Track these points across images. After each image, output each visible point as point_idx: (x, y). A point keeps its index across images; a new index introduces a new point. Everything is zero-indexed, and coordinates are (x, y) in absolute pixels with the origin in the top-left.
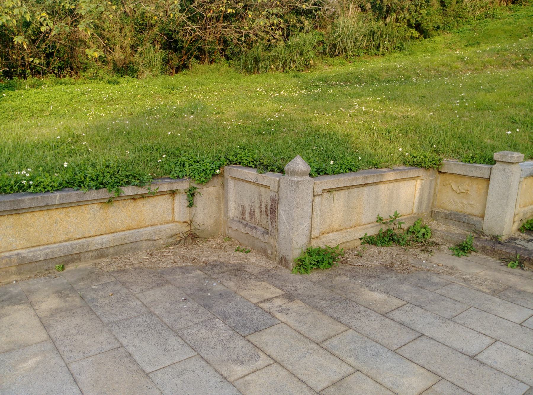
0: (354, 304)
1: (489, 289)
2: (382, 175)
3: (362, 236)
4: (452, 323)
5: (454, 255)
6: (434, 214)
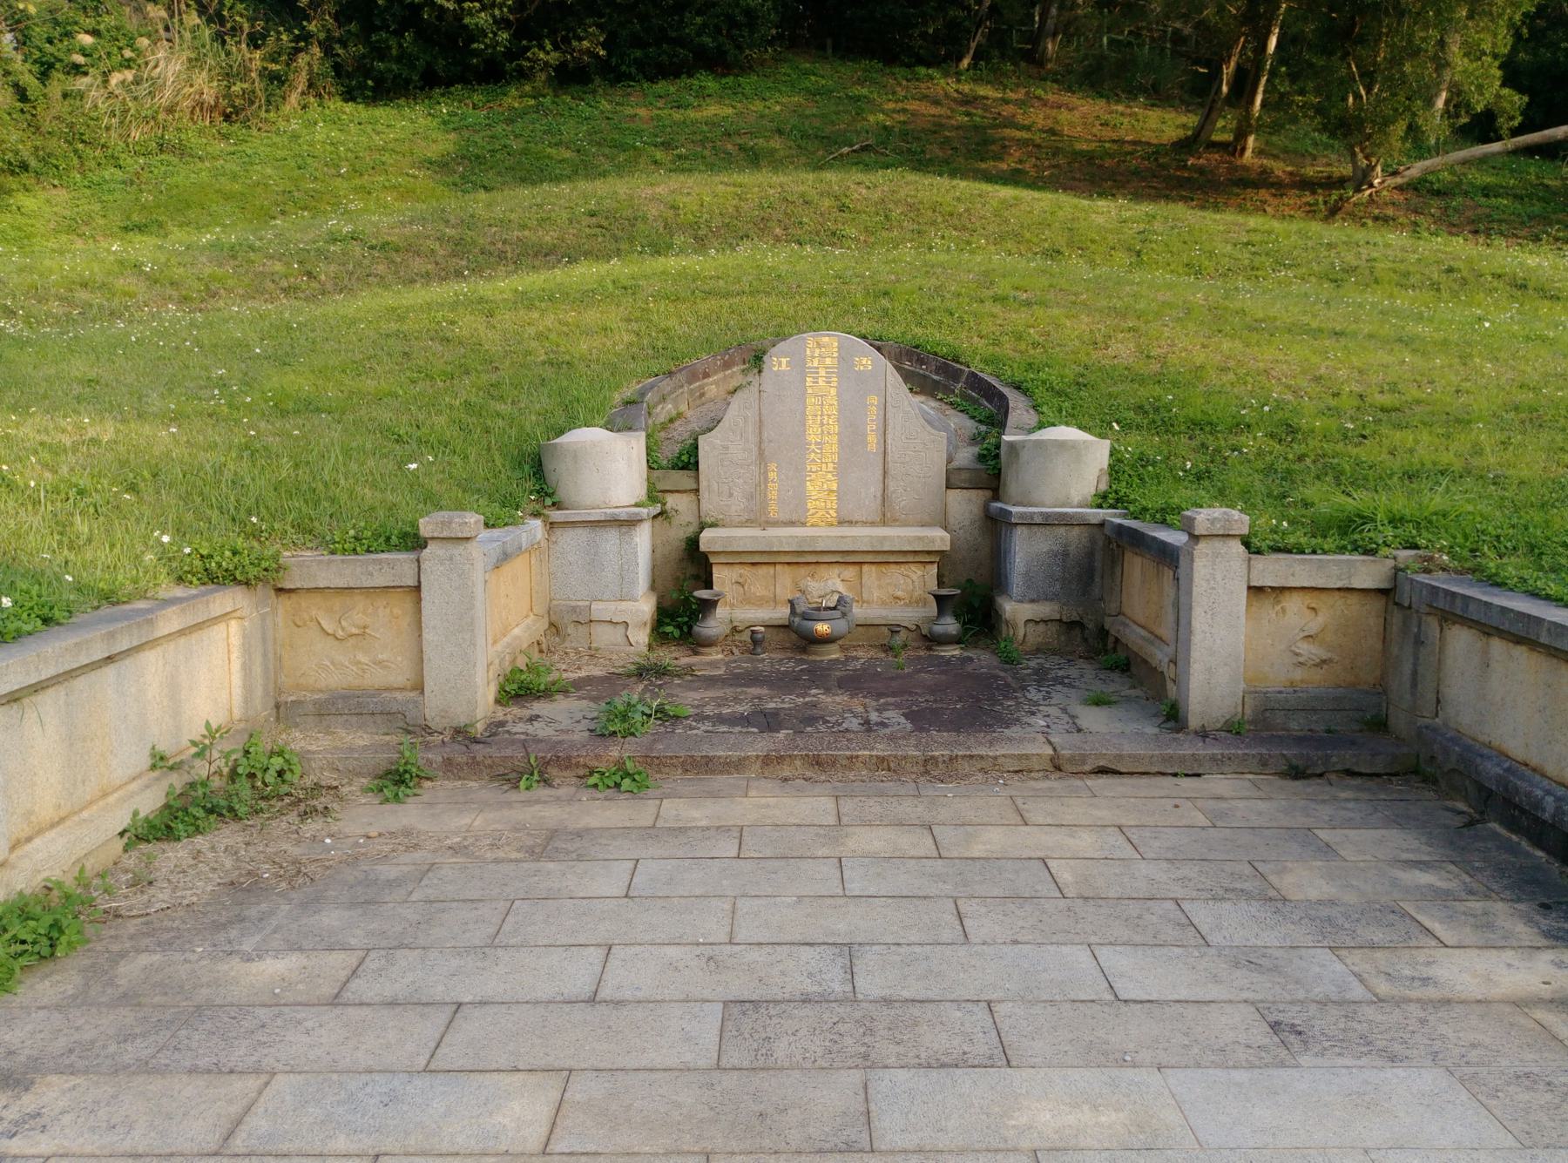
1: (518, 850)
2: (150, 622)
4: (500, 952)
5: (387, 800)
6: (284, 711)
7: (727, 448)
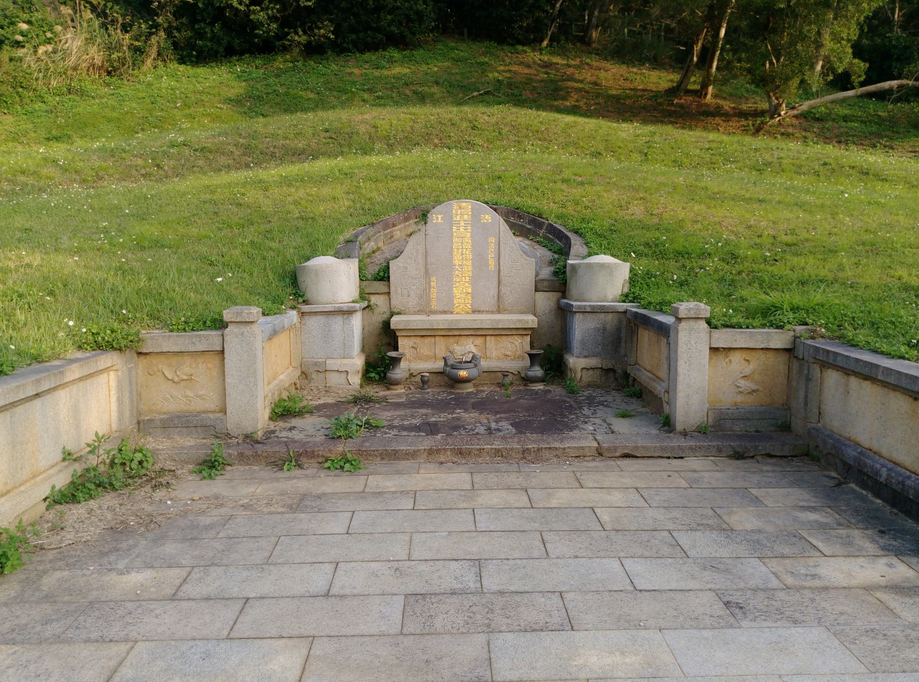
0: (112, 605)
1: (283, 507)
2: (62, 373)
3: (47, 492)
4: (272, 567)
5: (204, 478)
6: (142, 425)
7: (406, 268)
